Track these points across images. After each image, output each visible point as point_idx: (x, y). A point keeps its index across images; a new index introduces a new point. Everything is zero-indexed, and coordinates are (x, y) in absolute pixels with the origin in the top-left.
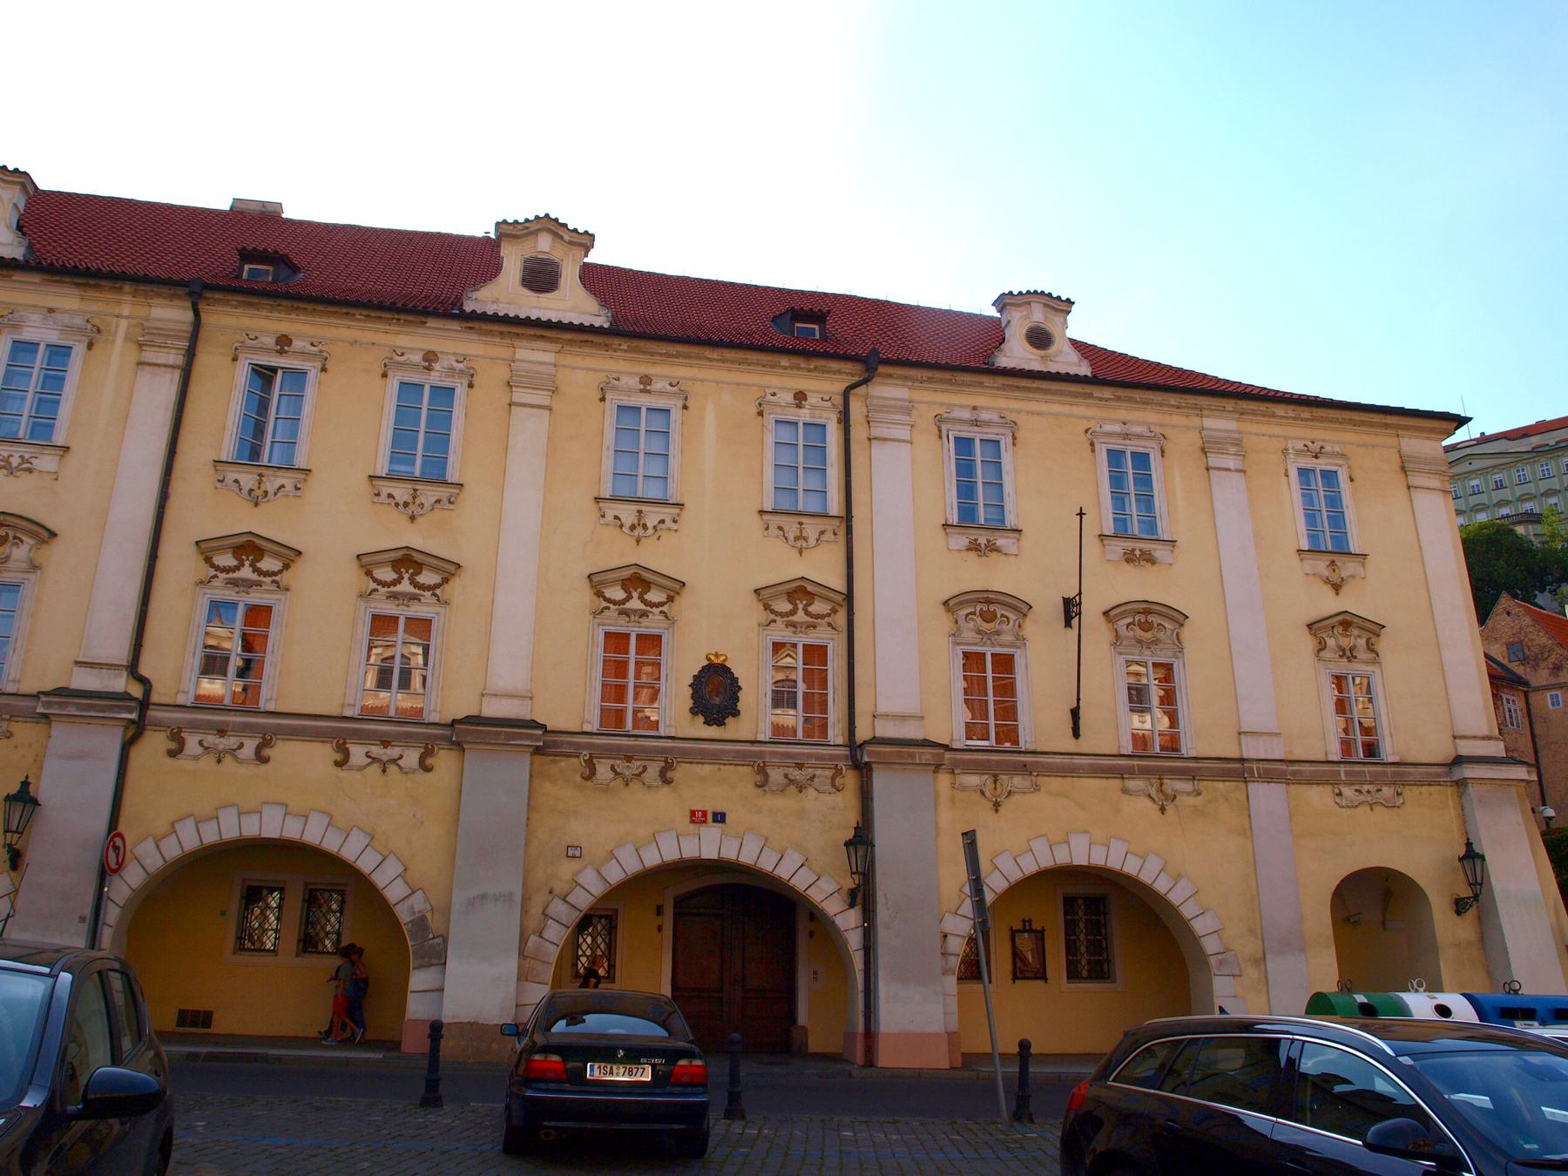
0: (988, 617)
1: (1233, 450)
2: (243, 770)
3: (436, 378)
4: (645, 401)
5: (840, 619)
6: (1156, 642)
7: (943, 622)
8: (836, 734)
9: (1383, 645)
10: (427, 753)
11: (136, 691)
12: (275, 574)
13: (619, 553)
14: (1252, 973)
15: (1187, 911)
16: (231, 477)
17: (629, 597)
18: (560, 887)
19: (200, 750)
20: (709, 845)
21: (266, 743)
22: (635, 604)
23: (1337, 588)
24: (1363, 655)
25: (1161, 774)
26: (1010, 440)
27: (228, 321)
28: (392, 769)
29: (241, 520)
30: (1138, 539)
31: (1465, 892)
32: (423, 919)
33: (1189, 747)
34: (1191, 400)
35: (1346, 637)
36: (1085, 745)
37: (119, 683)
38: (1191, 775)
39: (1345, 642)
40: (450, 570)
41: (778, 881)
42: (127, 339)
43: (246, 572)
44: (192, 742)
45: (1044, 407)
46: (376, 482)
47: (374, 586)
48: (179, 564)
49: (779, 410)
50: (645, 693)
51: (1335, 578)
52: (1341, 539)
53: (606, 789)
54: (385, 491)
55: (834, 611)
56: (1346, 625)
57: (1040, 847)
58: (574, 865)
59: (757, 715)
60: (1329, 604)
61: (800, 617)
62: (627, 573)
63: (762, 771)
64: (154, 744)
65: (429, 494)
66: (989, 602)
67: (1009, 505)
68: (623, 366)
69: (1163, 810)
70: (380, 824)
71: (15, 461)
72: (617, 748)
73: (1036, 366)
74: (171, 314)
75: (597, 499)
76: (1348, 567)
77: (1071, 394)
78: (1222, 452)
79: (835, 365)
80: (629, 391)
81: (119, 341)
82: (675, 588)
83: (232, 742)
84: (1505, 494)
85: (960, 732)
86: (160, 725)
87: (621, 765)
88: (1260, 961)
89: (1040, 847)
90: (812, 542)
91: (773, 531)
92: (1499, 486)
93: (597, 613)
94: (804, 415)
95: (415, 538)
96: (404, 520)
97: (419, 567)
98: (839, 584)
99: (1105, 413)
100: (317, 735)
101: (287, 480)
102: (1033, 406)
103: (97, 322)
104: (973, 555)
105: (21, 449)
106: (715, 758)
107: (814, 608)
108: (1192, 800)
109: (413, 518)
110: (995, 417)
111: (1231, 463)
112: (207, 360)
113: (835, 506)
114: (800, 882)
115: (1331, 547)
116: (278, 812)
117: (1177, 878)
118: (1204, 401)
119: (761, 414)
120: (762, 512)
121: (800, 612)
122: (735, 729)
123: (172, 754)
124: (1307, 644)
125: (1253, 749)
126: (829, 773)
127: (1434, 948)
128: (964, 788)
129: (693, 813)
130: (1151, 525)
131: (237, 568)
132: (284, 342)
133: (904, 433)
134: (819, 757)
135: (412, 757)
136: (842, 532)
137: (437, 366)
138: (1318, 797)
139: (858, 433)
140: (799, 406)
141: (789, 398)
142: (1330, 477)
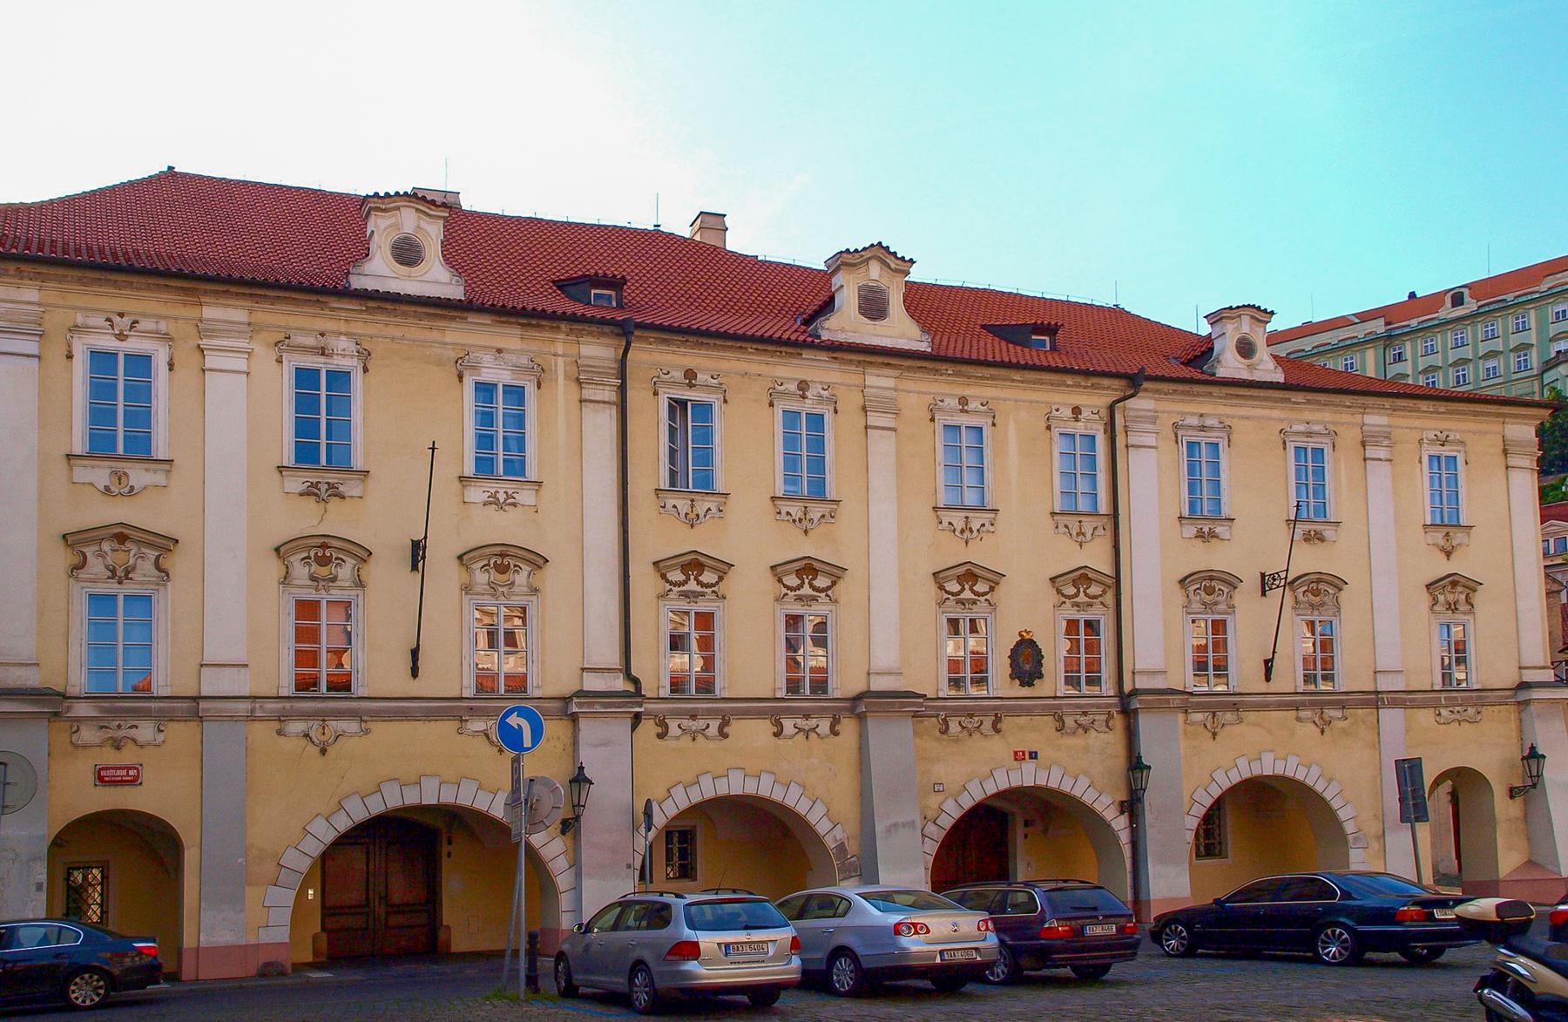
0: (1210, 591)
1: (1386, 443)
2: (711, 745)
3: (809, 406)
4: (963, 420)
5: (1109, 598)
6: (1323, 604)
7: (1178, 597)
8: (1108, 687)
9: (1477, 599)
10: (835, 722)
12: (713, 585)
13: (954, 553)
14: (1375, 845)
16: (670, 503)
17: (963, 589)
18: (931, 814)
19: (679, 732)
20: (1028, 775)
21: (725, 723)
22: (967, 594)
23: (1448, 554)
24: (1463, 607)
26: (360, 370)
27: (647, 356)
28: (813, 735)
29: (684, 541)
30: (1309, 520)
35: (1453, 592)
36: (1274, 686)
37: (619, 684)
38: (1342, 705)
39: (1451, 598)
40: (837, 573)
42: (567, 377)
43: (692, 586)
44: (673, 725)
46: (778, 502)
47: (785, 591)
48: (644, 583)
49: (1061, 424)
50: (513, 444)
53: (957, 740)
55: (1104, 592)
56: (1454, 584)
57: (1242, 763)
58: (940, 798)
60: (1442, 567)
61: (1082, 598)
62: (962, 570)
63: (1061, 719)
64: (648, 727)
65: (816, 511)
66: (1211, 578)
67: (1224, 499)
68: (945, 388)
69: (1322, 732)
70: (804, 775)
71: (502, 497)
73: (1245, 375)
75: (935, 509)
76: (1458, 537)
79: (1106, 382)
80: (951, 412)
82: (995, 579)
83: (701, 724)
87: (966, 722)
88: (1382, 836)
90: (1089, 536)
91: (1062, 529)
93: (780, 599)
94: (1079, 428)
96: (799, 533)
98: (1107, 568)
102: (1242, 411)
103: (538, 360)
106: (1028, 711)
107: (817, 583)
109: (806, 532)
112: (638, 396)
113: (1104, 506)
114: (1088, 799)
115: (1448, 527)
117: (1330, 781)
119: (1049, 428)
120: (1053, 514)
121: (806, 585)
122: (1042, 688)
123: (661, 736)
124: (1425, 599)
125: (1385, 684)
126: (1104, 717)
127: (1492, 822)
128: (1192, 724)
129: (1016, 753)
130: (1322, 509)
131: (685, 582)
132: (690, 375)
134: (1098, 706)
135: (824, 726)
136: (1110, 527)
137: (808, 394)
138: (1425, 717)
139: (1120, 441)
140: (1077, 420)
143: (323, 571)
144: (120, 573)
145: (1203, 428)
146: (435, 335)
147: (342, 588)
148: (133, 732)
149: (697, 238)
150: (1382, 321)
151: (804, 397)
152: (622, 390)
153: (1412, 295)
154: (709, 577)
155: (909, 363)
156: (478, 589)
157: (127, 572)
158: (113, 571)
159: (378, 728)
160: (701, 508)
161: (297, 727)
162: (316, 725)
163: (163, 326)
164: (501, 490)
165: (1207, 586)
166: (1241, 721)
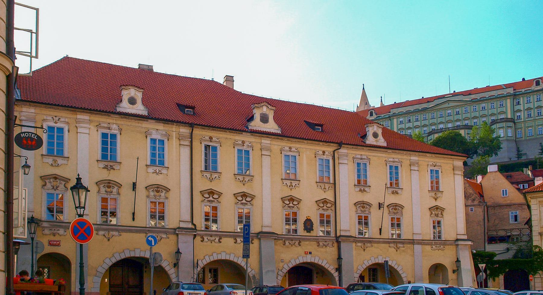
0: (363, 207)
2: (216, 244)
5: (333, 208)
7: (354, 208)
8: (333, 234)
11: (193, 227)
13: (287, 192)
15: (400, 272)
18: (280, 268)
20: (309, 259)
21: (220, 239)
22: (291, 205)
23: (436, 199)
25: (397, 243)
27: (197, 132)
28: (213, 242)
29: (208, 186)
30: (394, 185)
31: (455, 269)
32: (254, 276)
33: (403, 237)
34: (409, 152)
36: (382, 237)
37: (190, 226)
39: (436, 213)
40: (253, 197)
41: (322, 266)
43: (211, 198)
44: (205, 238)
45: (376, 154)
46: (284, 181)
48: (197, 197)
51: (436, 197)
52: (438, 188)
54: (237, 178)
56: (437, 208)
57: (372, 259)
58: (283, 264)
59: (318, 231)
61: (325, 207)
63: (318, 243)
64: (198, 238)
66: (364, 204)
67: (368, 180)
68: (285, 144)
72: (290, 239)
73: (375, 143)
74: (185, 130)
76: (439, 195)
77: (383, 151)
78: (414, 165)
79: (332, 144)
81: (174, 138)
82: (299, 201)
83: (213, 238)
84: (459, 117)
85: (357, 234)
86: (199, 235)
87: (291, 242)
89: (372, 259)
91: (319, 187)
92: (458, 113)
94: (325, 157)
95: (244, 189)
97: (247, 196)
98: (332, 199)
99: (389, 156)
100: (230, 236)
101: (217, 175)
102: (374, 154)
104: (360, 192)
105: (158, 168)
107: (247, 199)
108: (403, 249)
110: (365, 157)
111: (416, 168)
112: (196, 144)
113: (332, 181)
114: (326, 266)
115: (435, 188)
116: (225, 253)
118: (412, 153)
120: (234, 174)
122: (313, 233)
124: (428, 213)
128: (358, 246)
131: (209, 198)
132: (211, 138)
133: (346, 162)
134: (330, 240)
136: (333, 187)
138: (428, 248)
140: (324, 155)
141: (321, 153)
142: (437, 172)
143: (109, 190)
144: (55, 188)
145: (361, 159)
146: (140, 125)
147: (114, 195)
148: (58, 232)
149: (225, 84)
150: (512, 89)
151: (243, 145)
152: (191, 142)
153: (523, 79)
154: (216, 196)
155: (273, 137)
156: (151, 197)
157: (57, 187)
158: (53, 187)
159: (124, 234)
160: (213, 177)
161: (101, 233)
162: (107, 232)
163: (67, 120)
164: (158, 169)
165: (362, 205)
166: (372, 246)
